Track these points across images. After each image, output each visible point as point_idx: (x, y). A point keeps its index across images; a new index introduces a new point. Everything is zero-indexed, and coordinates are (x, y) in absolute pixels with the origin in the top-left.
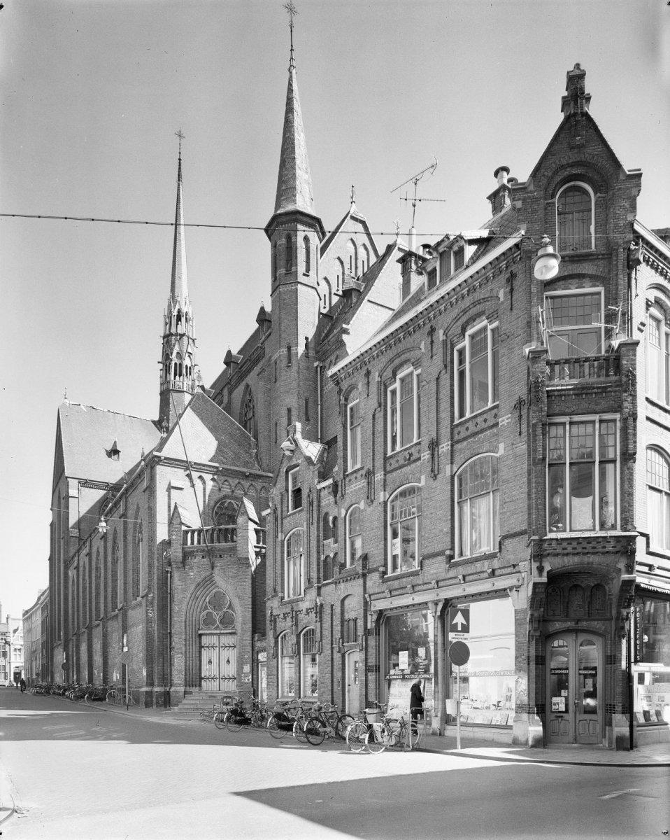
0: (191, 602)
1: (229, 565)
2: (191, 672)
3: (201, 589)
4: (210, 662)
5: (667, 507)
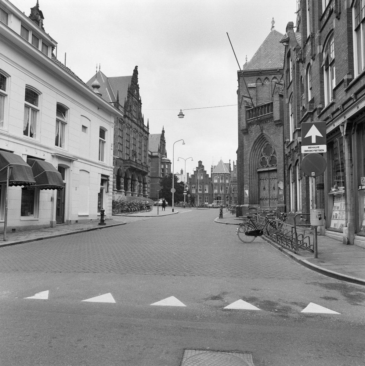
0: (252, 152)
1: (271, 127)
2: (253, 195)
3: (258, 144)
4: (264, 188)
5: (23, 19)
